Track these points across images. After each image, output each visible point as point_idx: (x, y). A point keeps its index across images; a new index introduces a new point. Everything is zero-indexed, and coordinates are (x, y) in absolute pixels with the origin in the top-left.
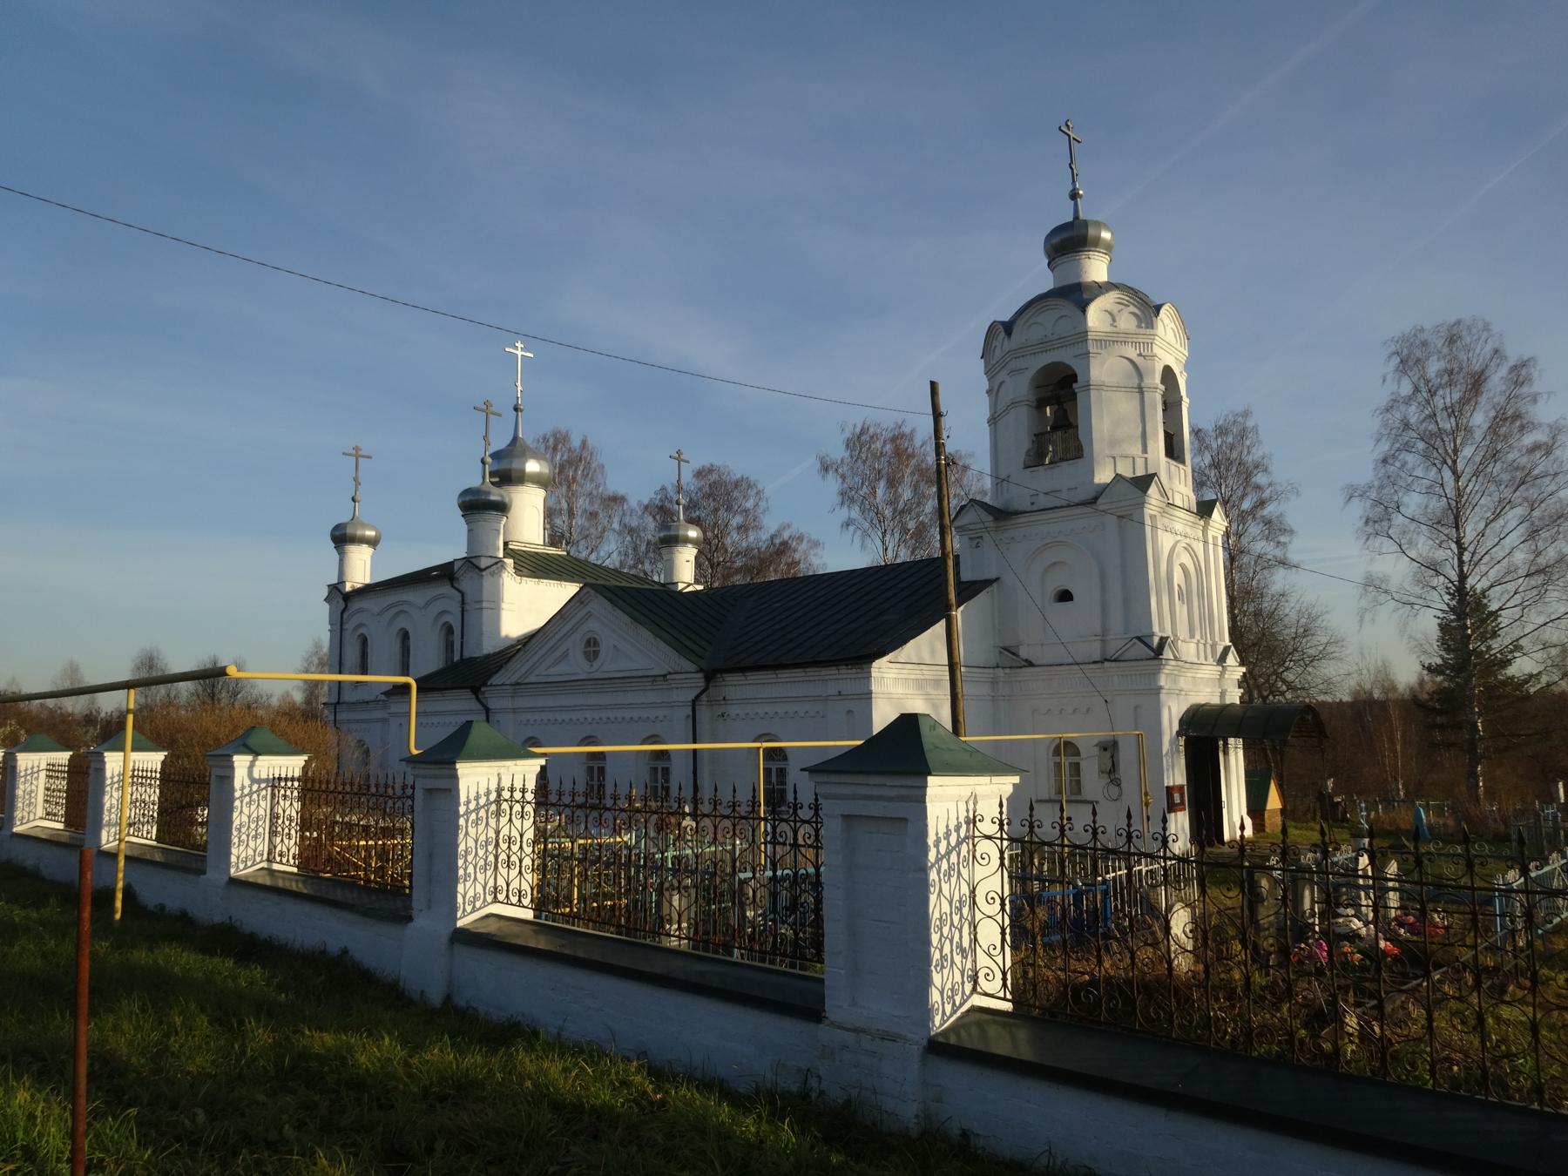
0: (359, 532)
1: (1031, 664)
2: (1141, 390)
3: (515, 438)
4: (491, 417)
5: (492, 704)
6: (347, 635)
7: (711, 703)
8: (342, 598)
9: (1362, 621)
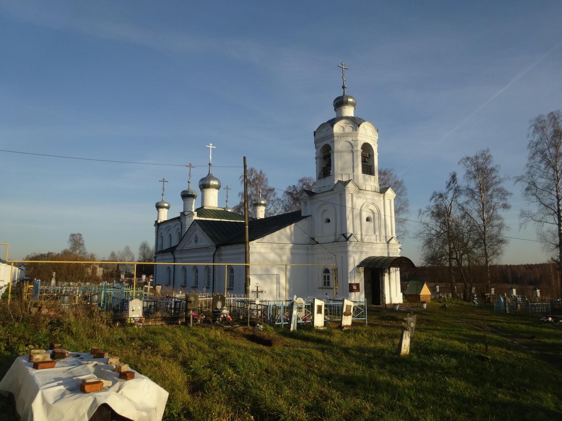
1: (317, 243)
2: (352, 152)
3: (209, 174)
5: (177, 256)
6: (159, 236)
7: (219, 255)
8: (158, 225)
9: (520, 228)
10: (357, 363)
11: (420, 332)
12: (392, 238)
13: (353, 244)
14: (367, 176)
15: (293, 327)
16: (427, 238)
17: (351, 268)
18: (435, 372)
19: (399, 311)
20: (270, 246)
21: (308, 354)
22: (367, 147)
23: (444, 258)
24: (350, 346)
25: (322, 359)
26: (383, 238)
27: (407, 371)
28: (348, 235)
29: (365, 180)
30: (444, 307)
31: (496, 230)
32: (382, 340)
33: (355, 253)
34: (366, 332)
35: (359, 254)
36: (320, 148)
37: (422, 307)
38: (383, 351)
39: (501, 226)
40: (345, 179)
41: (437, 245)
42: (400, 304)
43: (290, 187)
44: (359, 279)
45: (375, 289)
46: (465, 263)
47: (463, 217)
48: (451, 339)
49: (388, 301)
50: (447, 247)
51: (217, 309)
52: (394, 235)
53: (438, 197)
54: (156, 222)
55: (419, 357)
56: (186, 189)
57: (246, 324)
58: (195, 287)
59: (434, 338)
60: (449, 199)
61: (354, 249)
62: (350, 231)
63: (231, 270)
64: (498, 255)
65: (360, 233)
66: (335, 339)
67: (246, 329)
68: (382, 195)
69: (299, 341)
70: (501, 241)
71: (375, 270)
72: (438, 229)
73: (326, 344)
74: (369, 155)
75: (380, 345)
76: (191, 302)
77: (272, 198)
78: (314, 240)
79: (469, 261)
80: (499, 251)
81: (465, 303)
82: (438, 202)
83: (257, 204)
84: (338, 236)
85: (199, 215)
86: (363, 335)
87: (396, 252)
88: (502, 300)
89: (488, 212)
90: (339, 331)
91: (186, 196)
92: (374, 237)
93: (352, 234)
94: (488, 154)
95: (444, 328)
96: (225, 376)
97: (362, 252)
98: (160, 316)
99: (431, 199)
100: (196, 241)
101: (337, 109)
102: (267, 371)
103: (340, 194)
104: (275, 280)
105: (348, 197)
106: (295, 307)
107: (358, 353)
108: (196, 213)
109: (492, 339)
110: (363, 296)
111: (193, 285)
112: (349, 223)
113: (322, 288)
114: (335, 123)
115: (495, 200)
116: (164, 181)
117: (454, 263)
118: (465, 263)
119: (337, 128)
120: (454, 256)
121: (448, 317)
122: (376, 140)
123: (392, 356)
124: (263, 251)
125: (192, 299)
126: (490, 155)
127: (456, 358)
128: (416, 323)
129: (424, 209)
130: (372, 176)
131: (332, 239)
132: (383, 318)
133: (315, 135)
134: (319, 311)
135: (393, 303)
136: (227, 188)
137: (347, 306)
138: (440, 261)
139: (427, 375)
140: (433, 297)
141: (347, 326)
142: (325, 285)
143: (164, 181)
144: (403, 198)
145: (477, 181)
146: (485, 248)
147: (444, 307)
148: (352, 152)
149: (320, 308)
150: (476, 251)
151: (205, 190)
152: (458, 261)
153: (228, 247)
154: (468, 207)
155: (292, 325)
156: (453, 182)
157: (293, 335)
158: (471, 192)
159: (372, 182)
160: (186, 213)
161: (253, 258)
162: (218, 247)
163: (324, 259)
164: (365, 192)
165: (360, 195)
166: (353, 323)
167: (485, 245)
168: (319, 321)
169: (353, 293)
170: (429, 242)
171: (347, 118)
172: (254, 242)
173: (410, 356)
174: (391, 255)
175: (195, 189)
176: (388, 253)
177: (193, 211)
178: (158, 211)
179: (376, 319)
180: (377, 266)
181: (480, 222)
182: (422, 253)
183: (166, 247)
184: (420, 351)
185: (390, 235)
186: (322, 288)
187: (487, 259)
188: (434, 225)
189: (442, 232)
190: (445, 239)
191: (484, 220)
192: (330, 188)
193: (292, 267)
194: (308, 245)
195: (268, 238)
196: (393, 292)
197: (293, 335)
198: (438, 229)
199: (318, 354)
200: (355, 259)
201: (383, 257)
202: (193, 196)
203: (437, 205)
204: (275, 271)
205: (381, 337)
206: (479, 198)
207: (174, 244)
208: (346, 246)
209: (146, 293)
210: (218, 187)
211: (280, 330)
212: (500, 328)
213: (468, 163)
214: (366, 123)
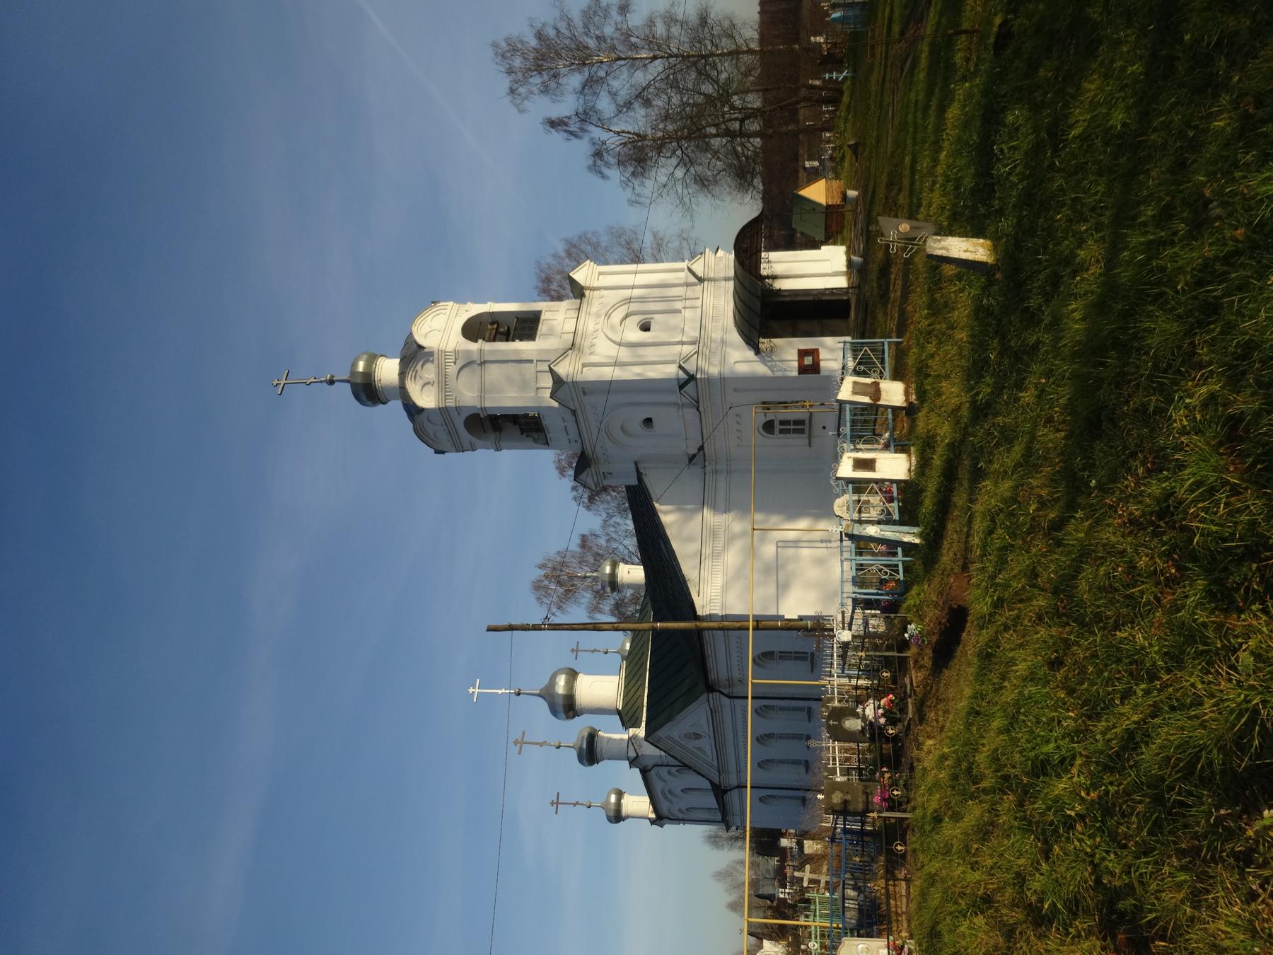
0: (613, 807)
1: (701, 448)
3: (539, 695)
4: (526, 739)
5: (734, 782)
8: (660, 819)
10: (1020, 386)
11: (920, 205)
12: (690, 270)
13: (703, 364)
14: (542, 328)
15: (910, 536)
16: (694, 188)
17: (760, 369)
18: (1052, 167)
19: (865, 256)
20: (707, 563)
21: (993, 521)
22: (473, 330)
23: (739, 149)
24: (966, 398)
25: (1006, 486)
26: (690, 292)
27: (1045, 248)
28: (682, 375)
29: (551, 334)
30: (855, 149)
31: (675, 30)
32: (946, 305)
33: (723, 360)
34: (922, 348)
35: (728, 350)
36: (474, 440)
37: (856, 199)
38: (980, 312)
39: (670, 20)
40: (548, 382)
41: (707, 165)
42: (848, 253)
43: (575, 499)
44: (788, 350)
45: (813, 313)
46: (754, 101)
47: (647, 103)
48: (939, 129)
49: (842, 282)
50: (716, 142)
51: (863, 731)
52: (683, 265)
53: (599, 162)
54: (653, 822)
55: (1001, 212)
56: (573, 754)
57: (903, 662)
58: (807, 765)
59: (939, 170)
60: (604, 136)
61: (716, 360)
62: (671, 371)
63: (764, 658)
64: (733, 26)
65: (678, 348)
66: (945, 432)
67: (916, 662)
68: (587, 293)
69: (950, 526)
70: (703, 20)
71: (766, 312)
72: (674, 161)
73: (958, 456)
74: (492, 324)
75: (962, 313)
76: (845, 802)
77: (602, 542)
78: (694, 456)
79: (747, 91)
80: (726, 24)
81: (845, 99)
82: (612, 160)
83: (613, 584)
84: (684, 400)
85: (636, 724)
86: (932, 356)
87: (723, 262)
88: (836, 15)
89: (634, 47)
90: (921, 415)
91: (590, 753)
92: (688, 313)
93: (680, 367)
94: (504, 45)
95: (909, 148)
96: (1078, 808)
97: (723, 342)
98: (882, 883)
99: (603, 176)
100: (697, 736)
101: (383, 399)
102: (1055, 664)
103: (584, 393)
104: (791, 551)
105: (591, 375)
106: (857, 530)
107: (989, 380)
108: (632, 731)
109: (939, 24)
110: (829, 341)
111: (802, 769)
112: (653, 373)
113: (810, 438)
114: (414, 405)
115: (609, 30)
116: (558, 803)
117: (754, 126)
118: (754, 101)
119: (426, 399)
120: (737, 125)
121: (878, 140)
122: (456, 306)
123: (996, 288)
124: (718, 581)
125: (837, 798)
126: (506, 40)
127: (1004, 109)
128: (896, 216)
129: (628, 193)
130: (542, 317)
131: (690, 413)
132: (884, 297)
133: (443, 452)
134: (868, 465)
135: (845, 269)
136: (576, 651)
137: (855, 393)
138: (747, 158)
139: (1061, 189)
140: (831, 175)
141: (907, 393)
142: (802, 431)
143: (558, 803)
144: (604, 241)
145: (564, 71)
146: (718, 55)
147: (855, 149)
148: (483, 363)
149: (860, 464)
150: (724, 76)
151: (578, 707)
152: (747, 117)
153: (711, 664)
154: (624, 94)
155: (907, 539)
156: (566, 124)
157: (934, 538)
158: (591, 84)
159: (558, 317)
160: (632, 754)
161: (736, 605)
162: (711, 688)
163: (741, 434)
164: (580, 332)
165: (587, 343)
166: (896, 376)
167: (712, 55)
168: (894, 466)
169: (822, 364)
170: (703, 183)
171: (402, 374)
172: (698, 602)
173: (995, 239)
174: (732, 273)
175: (575, 730)
176: (726, 279)
177: (626, 737)
178: (628, 817)
179: (886, 314)
180: (757, 306)
181: (658, 66)
182: (728, 199)
183: (711, 801)
184: (982, 210)
185: (683, 276)
186: (810, 438)
187: (744, 52)
188: (666, 169)
189: (679, 152)
190: (697, 146)
191: (655, 58)
192: (569, 416)
193: (757, 509)
194: (705, 470)
195: (688, 569)
196: (819, 268)
197: (934, 538)
198: (674, 161)
199: (992, 493)
200: (740, 360)
201: (736, 292)
202: (592, 737)
203: (620, 163)
204: (769, 550)
205: (937, 309)
206: (605, 67)
207: (707, 785)
208: (709, 380)
209: (823, 881)
210: (572, 675)
211: (919, 567)
212: (908, 12)
213: (522, 90)
214: (414, 329)
